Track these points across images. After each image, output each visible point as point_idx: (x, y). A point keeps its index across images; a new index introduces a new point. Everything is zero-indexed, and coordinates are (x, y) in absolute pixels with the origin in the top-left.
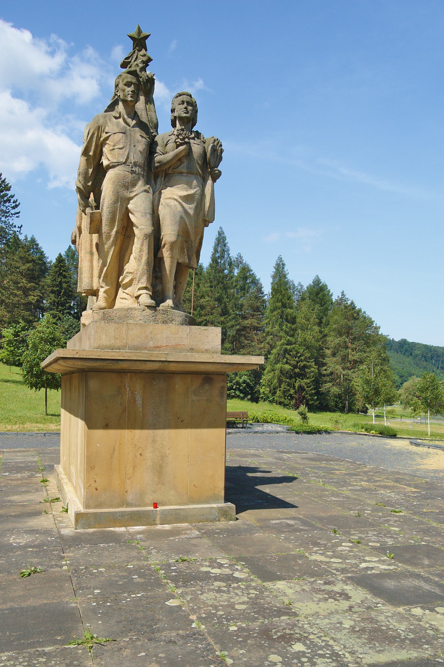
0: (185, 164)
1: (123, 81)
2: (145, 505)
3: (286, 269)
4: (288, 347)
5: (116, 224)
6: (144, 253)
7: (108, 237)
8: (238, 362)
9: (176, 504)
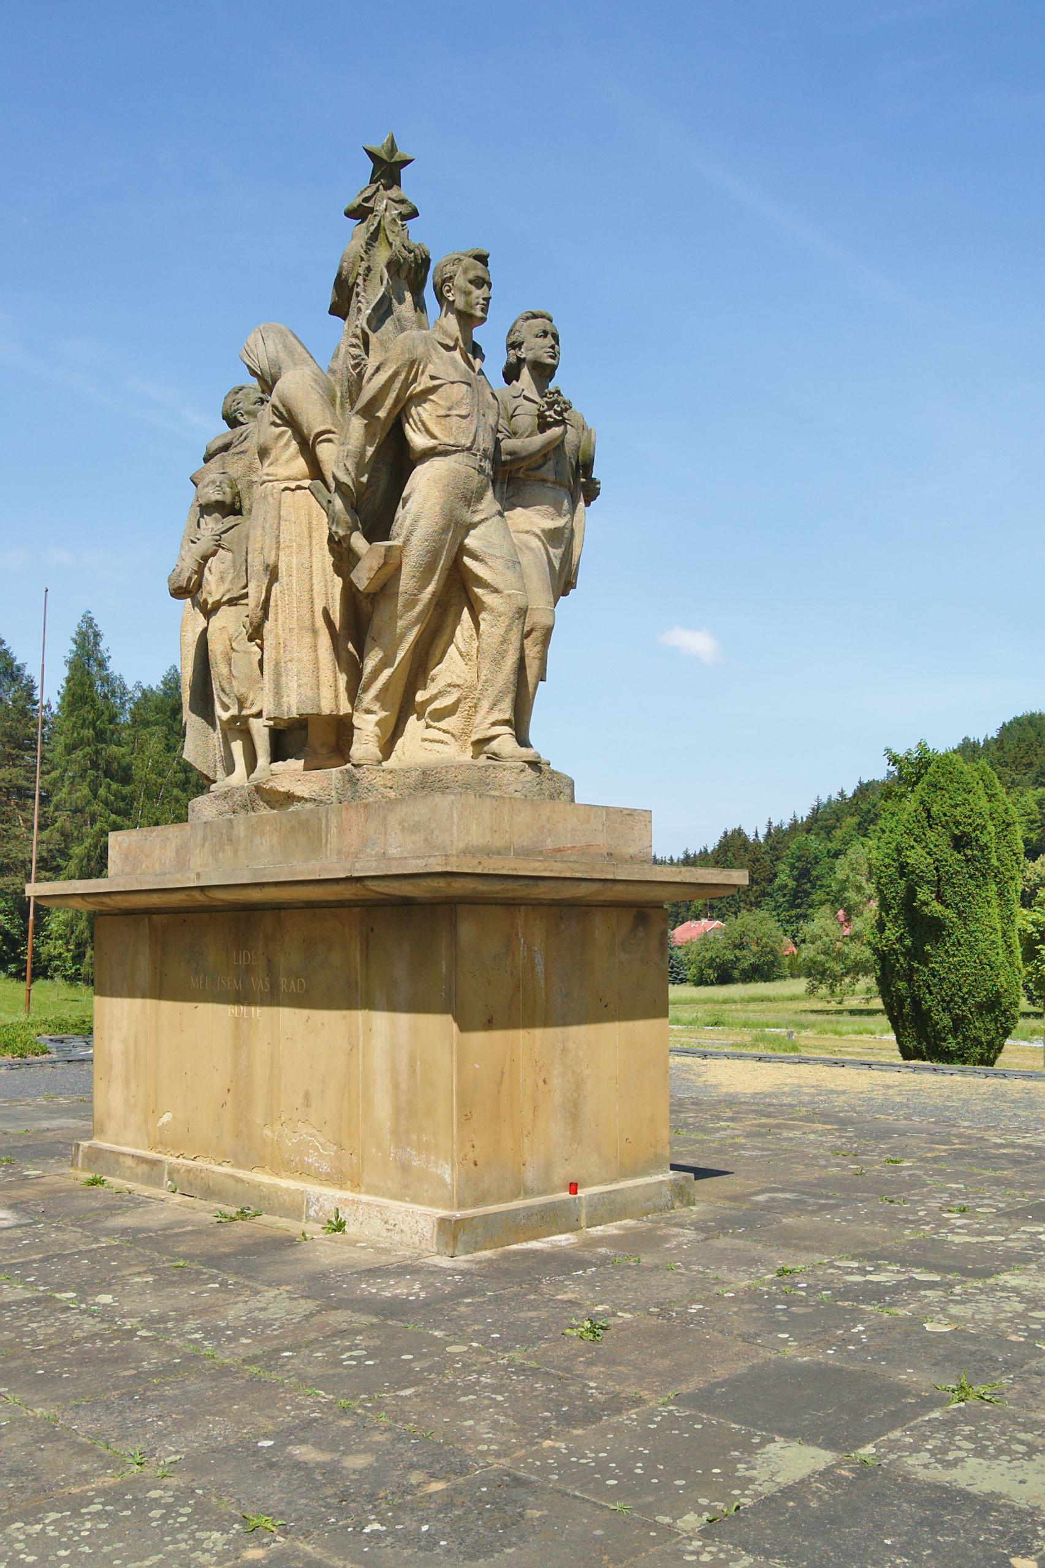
0: (550, 464)
1: (465, 272)
2: (553, 1191)
3: (103, 646)
5: (436, 577)
6: (511, 647)
7: (412, 603)
8: (714, 882)
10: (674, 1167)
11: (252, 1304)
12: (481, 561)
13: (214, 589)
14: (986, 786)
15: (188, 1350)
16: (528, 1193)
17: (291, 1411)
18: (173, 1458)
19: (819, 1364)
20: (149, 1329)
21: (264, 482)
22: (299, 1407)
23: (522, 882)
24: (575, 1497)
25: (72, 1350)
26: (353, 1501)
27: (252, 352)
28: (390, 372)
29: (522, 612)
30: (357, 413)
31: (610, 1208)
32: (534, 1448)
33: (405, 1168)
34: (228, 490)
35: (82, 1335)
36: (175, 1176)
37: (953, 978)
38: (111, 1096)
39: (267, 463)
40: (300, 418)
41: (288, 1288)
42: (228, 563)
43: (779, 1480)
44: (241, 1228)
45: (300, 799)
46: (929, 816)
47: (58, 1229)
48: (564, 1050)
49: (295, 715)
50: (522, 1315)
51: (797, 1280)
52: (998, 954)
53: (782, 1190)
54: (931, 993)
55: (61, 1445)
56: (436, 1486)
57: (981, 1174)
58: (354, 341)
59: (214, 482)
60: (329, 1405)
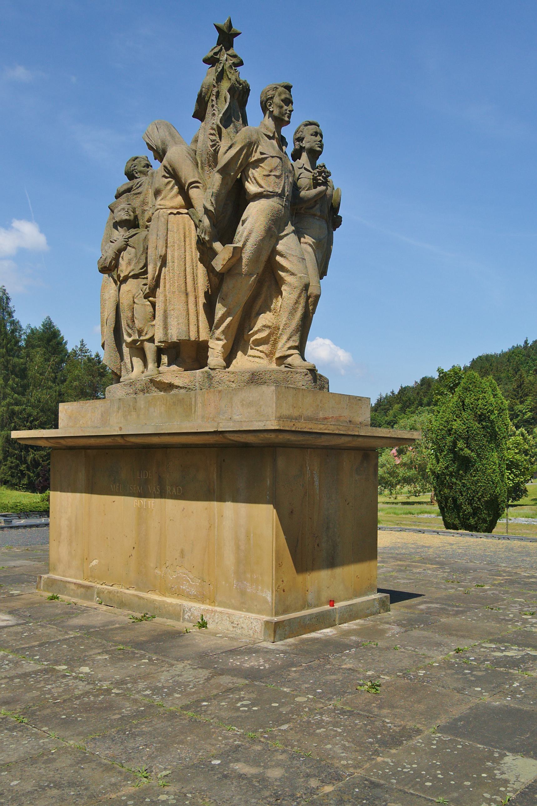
0: (318, 206)
1: (280, 95)
3: (11, 305)
4: (16, 408)
8: (406, 437)
9: (343, 600)
10: (380, 591)
11: (172, 672)
12: (285, 257)
13: (124, 269)
14: (492, 390)
15: (146, 702)
16: (310, 606)
17: (222, 740)
18: (164, 773)
19: (505, 706)
20: (118, 689)
21: (158, 209)
22: (226, 738)
23: (314, 436)
24: (412, 794)
25: (77, 702)
26: (283, 799)
27: (151, 136)
28: (238, 149)
29: (306, 287)
30: (218, 171)
31: (351, 614)
32: (373, 762)
33: (243, 593)
34: (132, 214)
35: (80, 692)
36: (101, 595)
37: (473, 487)
38: (60, 550)
39: (159, 198)
40: (180, 173)
41: (189, 662)
42: (133, 255)
43: (522, 780)
44: (146, 625)
45: (177, 387)
46: (463, 404)
47: (42, 626)
48: (328, 528)
49: (175, 339)
50: (328, 677)
51: (467, 655)
52: (496, 476)
53: (432, 603)
54: (462, 495)
55: (93, 765)
56: (328, 789)
57: (529, 593)
58: (212, 132)
59: (124, 209)
60: (242, 736)
